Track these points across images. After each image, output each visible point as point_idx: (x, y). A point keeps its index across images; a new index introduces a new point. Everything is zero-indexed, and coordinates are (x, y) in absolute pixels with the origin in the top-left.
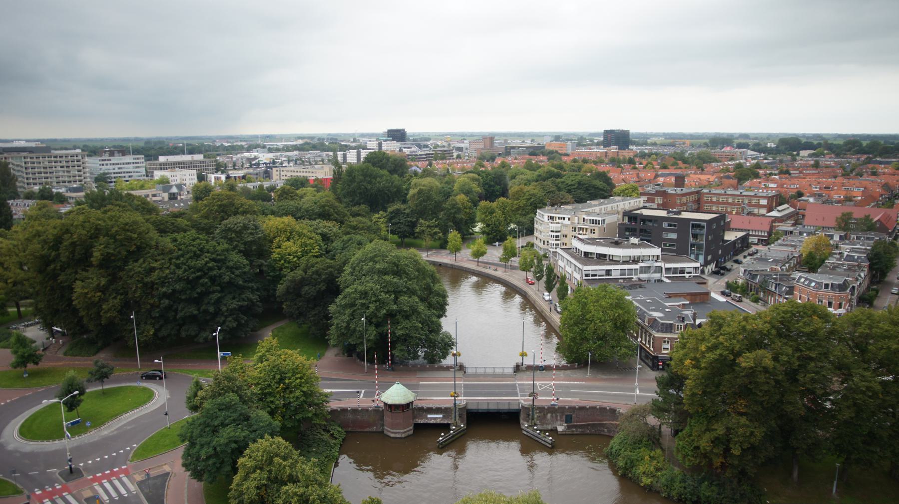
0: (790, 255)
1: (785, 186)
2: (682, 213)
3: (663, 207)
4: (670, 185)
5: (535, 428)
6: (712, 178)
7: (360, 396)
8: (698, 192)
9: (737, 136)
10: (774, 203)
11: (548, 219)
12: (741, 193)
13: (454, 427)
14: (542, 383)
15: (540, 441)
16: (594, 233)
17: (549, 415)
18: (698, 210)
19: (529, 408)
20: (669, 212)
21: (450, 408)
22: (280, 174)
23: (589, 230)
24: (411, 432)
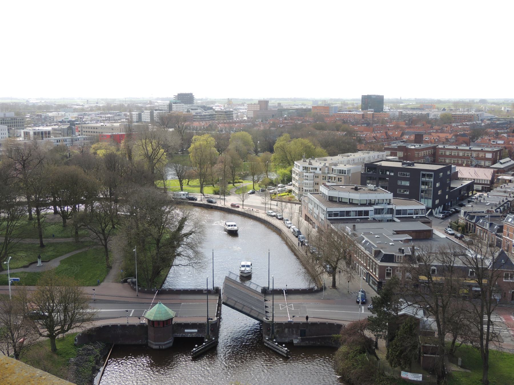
0: (504, 199)
1: (511, 143)
2: (415, 164)
3: (400, 160)
5: (274, 340)
6: (449, 136)
8: (434, 148)
9: (478, 101)
10: (498, 157)
11: (303, 170)
12: (470, 148)
13: (206, 340)
15: (278, 351)
16: (341, 181)
17: (286, 330)
18: (434, 162)
19: (269, 324)
20: (403, 164)
21: (203, 324)
22: (82, 130)
23: (337, 179)
24: (171, 344)
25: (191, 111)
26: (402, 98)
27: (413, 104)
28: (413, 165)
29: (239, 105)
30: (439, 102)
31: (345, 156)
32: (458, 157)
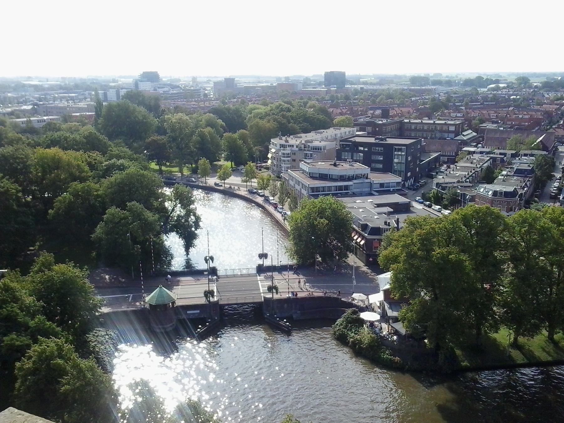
2: (387, 139)
4: (377, 117)
7: (129, 300)
10: (460, 129)
11: (280, 147)
12: (434, 122)
14: (280, 280)
18: (401, 136)
25: (158, 89)
26: (361, 74)
27: (373, 80)
28: (386, 141)
29: (205, 82)
30: (396, 76)
31: (319, 133)
32: (423, 130)
